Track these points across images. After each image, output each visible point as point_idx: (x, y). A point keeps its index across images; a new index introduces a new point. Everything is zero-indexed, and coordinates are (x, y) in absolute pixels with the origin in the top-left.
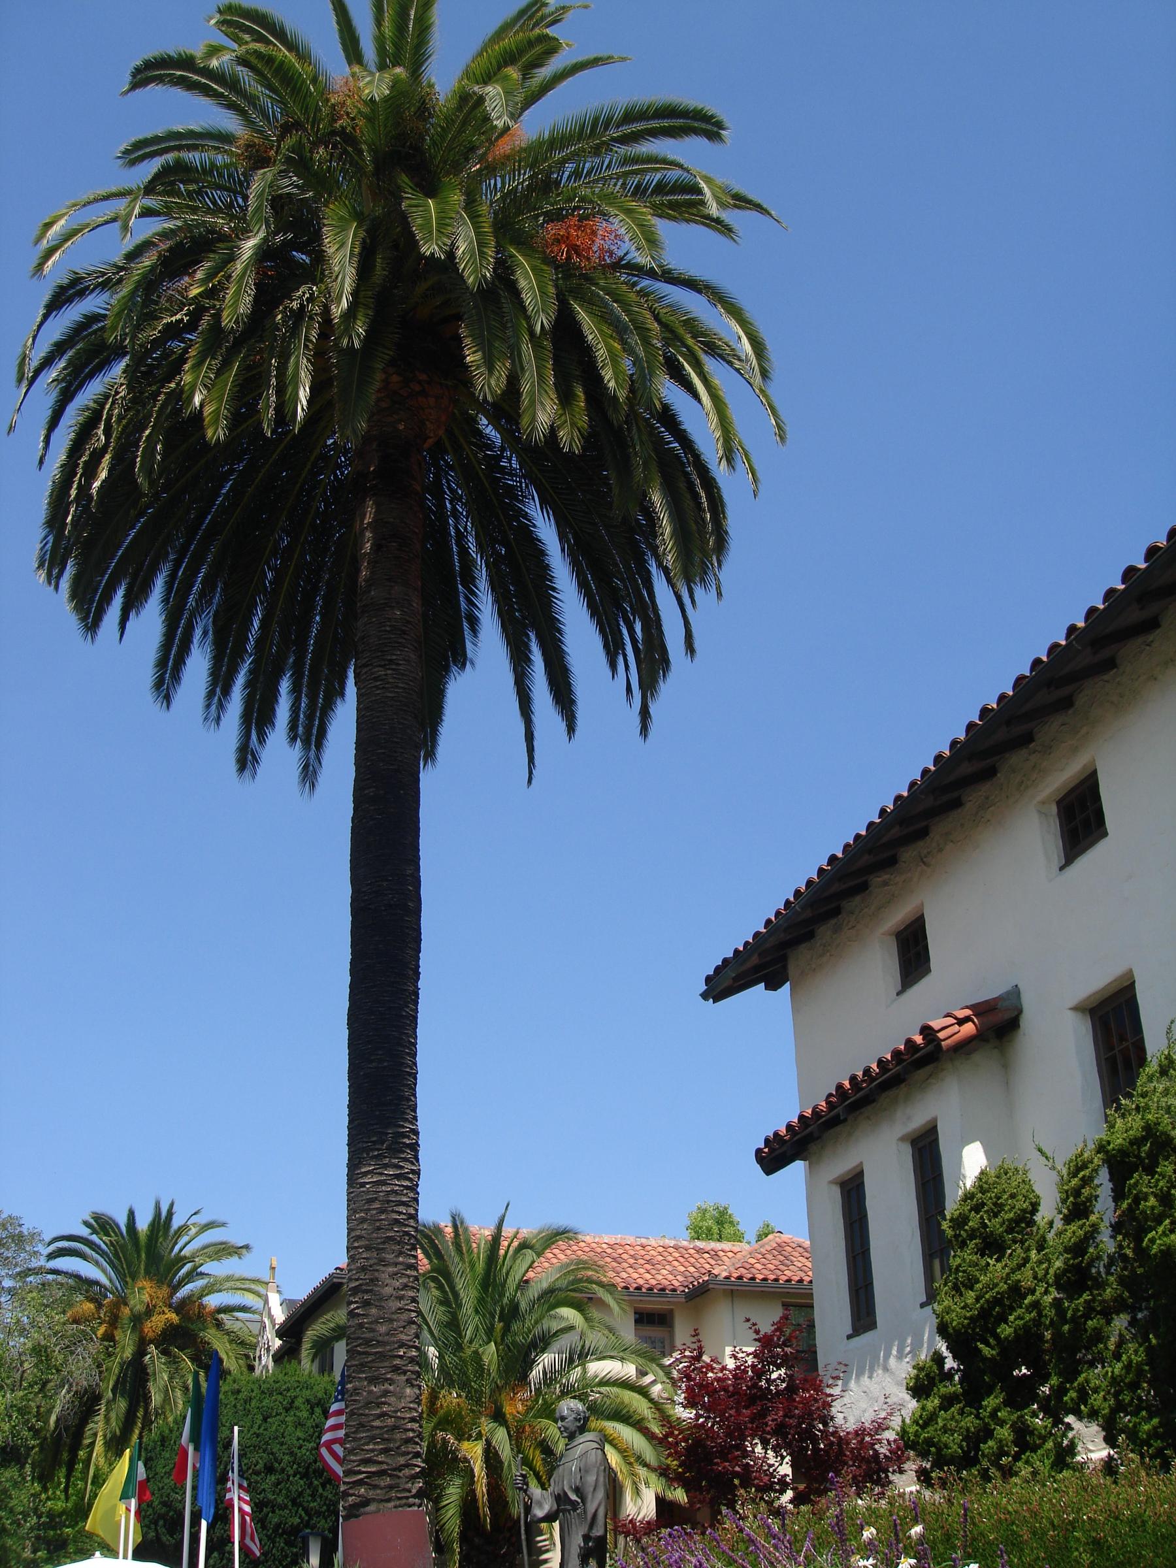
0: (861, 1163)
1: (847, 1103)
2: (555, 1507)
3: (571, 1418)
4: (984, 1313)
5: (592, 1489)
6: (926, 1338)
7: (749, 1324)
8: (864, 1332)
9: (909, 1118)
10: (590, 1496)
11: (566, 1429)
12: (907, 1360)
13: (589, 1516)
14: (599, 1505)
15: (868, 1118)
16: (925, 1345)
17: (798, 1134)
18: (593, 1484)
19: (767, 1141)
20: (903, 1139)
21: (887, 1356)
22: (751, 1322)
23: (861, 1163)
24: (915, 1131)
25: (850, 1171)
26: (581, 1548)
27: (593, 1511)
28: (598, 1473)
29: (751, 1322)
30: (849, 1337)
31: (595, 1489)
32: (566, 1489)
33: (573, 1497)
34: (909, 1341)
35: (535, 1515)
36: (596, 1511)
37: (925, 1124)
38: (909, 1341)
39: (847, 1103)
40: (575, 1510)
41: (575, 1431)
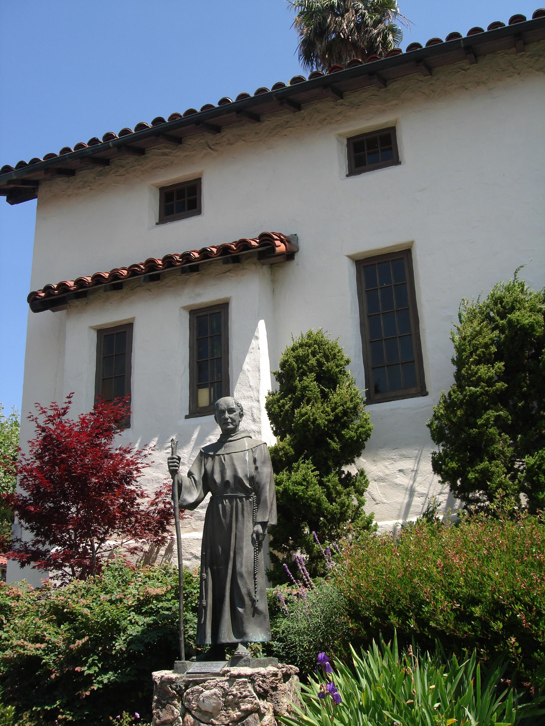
0: (134, 319)
4: (337, 418)
6: (195, 436)
9: (199, 295)
16: (192, 443)
20: (184, 308)
23: (134, 319)
25: (114, 323)
32: (241, 474)
40: (248, 498)
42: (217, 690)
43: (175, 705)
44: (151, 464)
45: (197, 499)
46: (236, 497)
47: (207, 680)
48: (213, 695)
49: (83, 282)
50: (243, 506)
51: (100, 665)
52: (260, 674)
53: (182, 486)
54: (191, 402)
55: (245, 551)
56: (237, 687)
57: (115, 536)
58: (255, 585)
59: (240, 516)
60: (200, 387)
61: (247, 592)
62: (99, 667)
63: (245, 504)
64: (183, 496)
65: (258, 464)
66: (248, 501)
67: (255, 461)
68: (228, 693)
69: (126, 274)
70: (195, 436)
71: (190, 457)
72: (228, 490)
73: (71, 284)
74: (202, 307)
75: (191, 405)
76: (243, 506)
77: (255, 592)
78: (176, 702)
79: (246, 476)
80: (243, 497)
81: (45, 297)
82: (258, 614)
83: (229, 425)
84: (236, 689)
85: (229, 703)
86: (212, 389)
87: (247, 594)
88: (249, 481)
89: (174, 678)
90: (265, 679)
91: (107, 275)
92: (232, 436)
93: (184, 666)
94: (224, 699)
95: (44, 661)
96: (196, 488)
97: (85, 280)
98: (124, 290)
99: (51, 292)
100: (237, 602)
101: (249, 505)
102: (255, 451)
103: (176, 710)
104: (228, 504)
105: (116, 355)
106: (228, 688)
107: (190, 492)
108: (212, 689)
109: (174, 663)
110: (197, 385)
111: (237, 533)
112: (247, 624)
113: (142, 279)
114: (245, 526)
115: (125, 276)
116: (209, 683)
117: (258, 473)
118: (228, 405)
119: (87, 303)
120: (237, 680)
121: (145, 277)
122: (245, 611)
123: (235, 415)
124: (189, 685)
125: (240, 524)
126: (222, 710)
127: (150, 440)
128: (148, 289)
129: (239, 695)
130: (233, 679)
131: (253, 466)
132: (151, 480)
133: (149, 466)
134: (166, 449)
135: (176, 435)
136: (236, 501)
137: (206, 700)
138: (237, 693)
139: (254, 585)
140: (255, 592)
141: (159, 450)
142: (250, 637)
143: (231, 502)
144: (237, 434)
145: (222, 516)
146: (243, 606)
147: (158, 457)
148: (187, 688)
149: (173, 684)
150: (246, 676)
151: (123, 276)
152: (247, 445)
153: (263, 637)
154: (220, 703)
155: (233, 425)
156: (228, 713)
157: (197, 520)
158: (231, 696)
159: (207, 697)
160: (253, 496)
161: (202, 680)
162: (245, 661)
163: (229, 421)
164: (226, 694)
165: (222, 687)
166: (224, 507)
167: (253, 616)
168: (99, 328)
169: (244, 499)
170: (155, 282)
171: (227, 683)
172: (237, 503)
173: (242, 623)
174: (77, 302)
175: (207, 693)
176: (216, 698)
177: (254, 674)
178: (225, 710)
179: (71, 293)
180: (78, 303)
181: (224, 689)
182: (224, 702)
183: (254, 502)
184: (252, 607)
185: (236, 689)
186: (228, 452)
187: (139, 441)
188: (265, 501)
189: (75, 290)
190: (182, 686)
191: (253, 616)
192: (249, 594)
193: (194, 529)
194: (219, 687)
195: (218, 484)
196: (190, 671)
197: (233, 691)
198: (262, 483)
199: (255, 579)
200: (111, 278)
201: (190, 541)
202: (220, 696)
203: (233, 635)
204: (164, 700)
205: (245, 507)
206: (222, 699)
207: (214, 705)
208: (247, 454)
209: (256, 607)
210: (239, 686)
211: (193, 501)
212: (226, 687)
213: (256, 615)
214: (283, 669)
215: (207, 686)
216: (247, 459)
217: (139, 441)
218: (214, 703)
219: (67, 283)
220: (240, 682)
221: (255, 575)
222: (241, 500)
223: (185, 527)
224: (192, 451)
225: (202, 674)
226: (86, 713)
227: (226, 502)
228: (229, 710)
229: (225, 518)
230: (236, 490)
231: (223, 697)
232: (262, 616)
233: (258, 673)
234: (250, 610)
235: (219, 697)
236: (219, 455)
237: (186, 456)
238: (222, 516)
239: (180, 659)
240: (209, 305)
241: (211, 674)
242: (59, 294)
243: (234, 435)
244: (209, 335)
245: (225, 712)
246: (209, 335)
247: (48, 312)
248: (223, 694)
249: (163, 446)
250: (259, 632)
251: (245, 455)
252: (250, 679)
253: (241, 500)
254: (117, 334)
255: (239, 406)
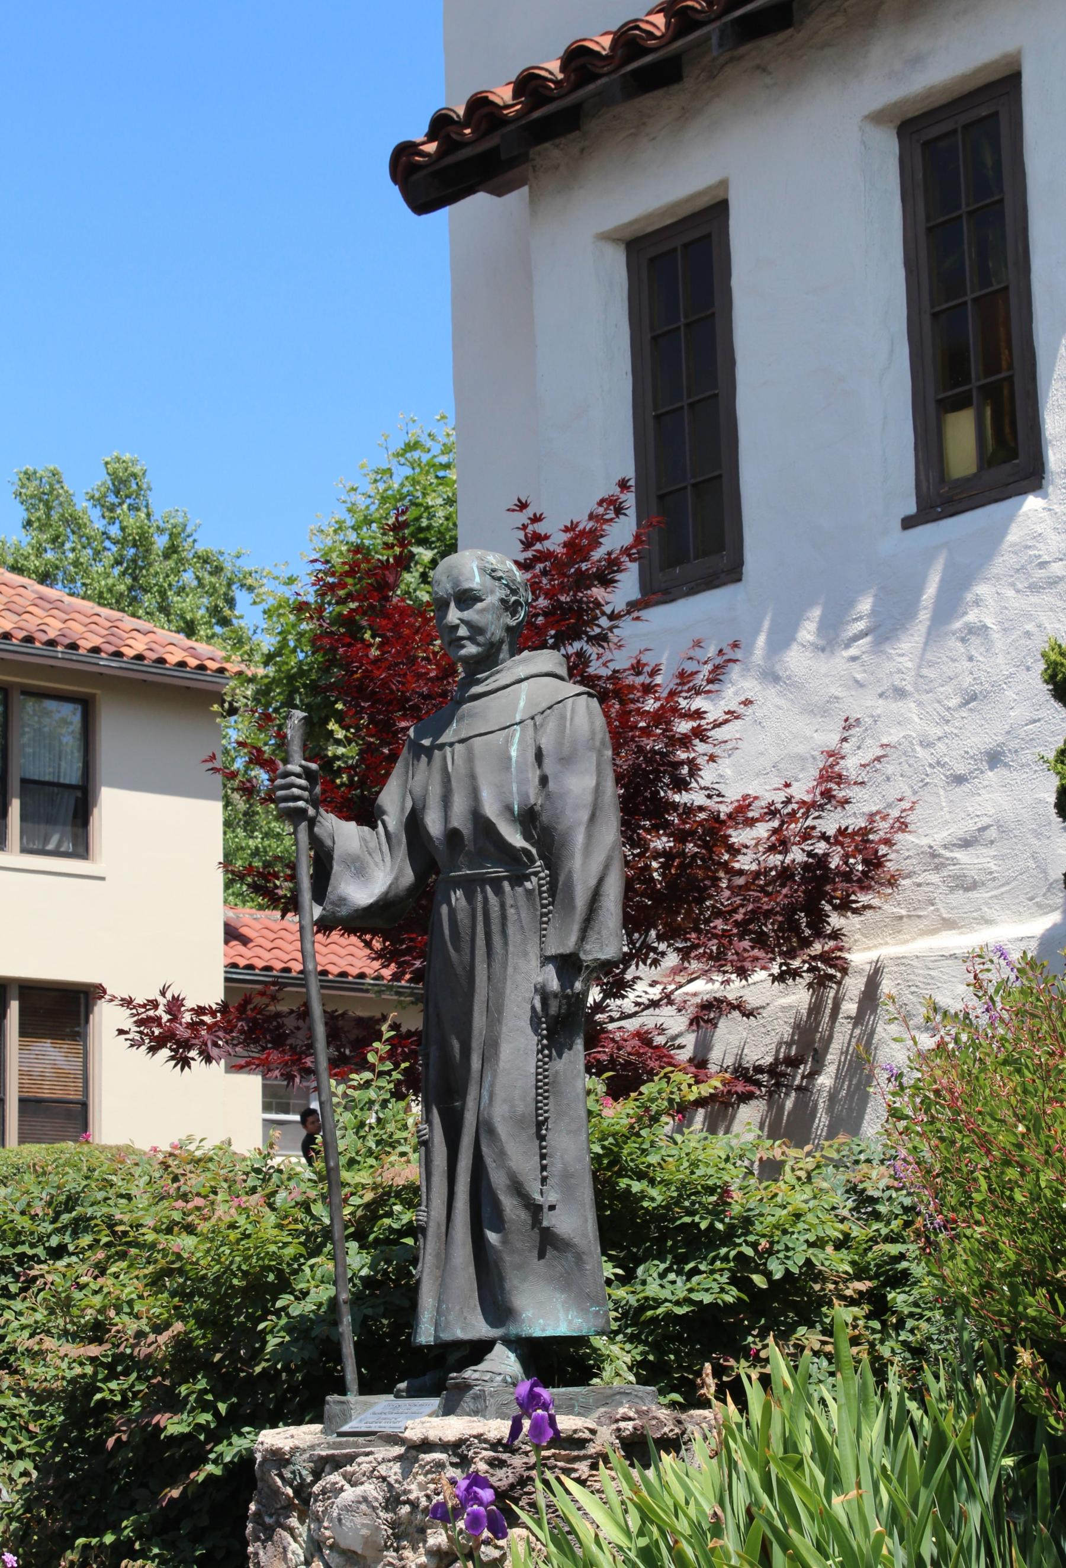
0: (724, 184)
1: (630, 67)
2: (409, 877)
3: (492, 600)
5: (584, 816)
6: (931, 591)
7: (522, 518)
8: (693, 591)
9: (917, 61)
10: (579, 838)
11: (476, 630)
12: (853, 651)
13: (581, 900)
14: (606, 867)
15: (763, 69)
16: (924, 616)
17: (550, 100)
18: (589, 798)
19: (441, 124)
20: (878, 118)
21: (781, 640)
22: (529, 512)
23: (724, 184)
24: (929, 93)
26: (545, 995)
27: (593, 882)
28: (598, 764)
29: (529, 512)
30: (908, 523)
31: (593, 818)
32: (491, 809)
33: (516, 839)
34: (865, 605)
35: (342, 901)
36: (601, 881)
37: (965, 78)
38: (865, 605)
39: (630, 67)
40: (517, 880)
41: (501, 642)
42: (372, 1486)
43: (291, 1530)
44: (741, 710)
45: (386, 893)
46: (482, 880)
47: (357, 1455)
48: (360, 1502)
49: (540, 82)
50: (503, 906)
51: (222, 1407)
52: (486, 1441)
53: (330, 858)
54: (921, 467)
55: (506, 1051)
56: (421, 1478)
57: (672, 959)
58: (543, 1157)
59: (497, 940)
60: (959, 404)
61: (508, 1182)
62: (216, 1414)
63: (509, 902)
64: (335, 888)
65: (550, 766)
66: (520, 890)
67: (539, 756)
68: (398, 1495)
69: (663, 28)
70: (931, 591)
71: (920, 667)
72: (461, 859)
73: (504, 94)
74: (937, 104)
75: (923, 477)
76: (503, 906)
77: (544, 1180)
78: (293, 1522)
79: (509, 808)
80: (500, 880)
81: (441, 153)
82: (556, 1248)
83: (463, 647)
84: (419, 1484)
85: (402, 1528)
86: (988, 412)
87: (508, 1187)
88: (522, 824)
89: (287, 1448)
90: (504, 1456)
91: (607, 41)
92: (479, 682)
93: (343, 1412)
94: (389, 1516)
95: (98, 1396)
96: (388, 858)
97: (543, 73)
98: (688, 83)
99: (454, 136)
100: (486, 1212)
101: (522, 901)
102: (542, 725)
103: (294, 1546)
104: (463, 902)
105: (687, 325)
106: (397, 1481)
107: (360, 870)
108: (362, 1483)
109: (323, 1402)
110: (939, 402)
111: (491, 994)
112: (516, 1282)
113: (714, 40)
114: (510, 970)
115: (663, 36)
116: (359, 1464)
117: (548, 796)
118: (456, 583)
119: (582, 151)
120: (422, 1456)
121: (722, 31)
122: (505, 1242)
123: (481, 611)
124: (323, 1471)
125: (496, 966)
126: (387, 1548)
127: (851, 603)
128: (758, 67)
129: (424, 1502)
130: (414, 1453)
131: (533, 776)
132: (811, 760)
133: (737, 718)
134: (847, 646)
135: (873, 591)
136: (484, 892)
137: (345, 1516)
138: (418, 1498)
139: (537, 1158)
140: (544, 1180)
141: (828, 649)
142: (527, 1323)
143: (470, 897)
144: (498, 672)
145: (449, 944)
146: (499, 1225)
147: (826, 675)
148: (317, 1475)
149: (285, 1467)
150: (443, 1446)
151: (655, 38)
152: (522, 704)
153: (570, 1322)
154: (378, 1528)
155: (478, 644)
156: (401, 1559)
157: (952, 889)
158: (407, 1506)
159: (347, 1508)
160: (536, 874)
161: (346, 1455)
162: (476, 1398)
163: (463, 631)
164: (393, 1501)
165: (384, 1479)
166: (452, 912)
167: (541, 1255)
168: (628, 235)
169: (506, 885)
170: (781, 37)
171: (397, 1467)
172: (486, 900)
173: (501, 1279)
174: (551, 152)
175: (350, 1494)
176: (369, 1511)
177: (467, 1440)
178: (396, 1550)
179: (512, 127)
180: (556, 153)
181: (389, 1485)
182: (393, 1525)
183: (541, 893)
184: (533, 1227)
185: (419, 1484)
186: (463, 736)
187: (766, 625)
188: (569, 886)
189: (520, 115)
190: (304, 1473)
191: (541, 1255)
192: (518, 1189)
193: (944, 919)
194: (377, 1478)
195: (437, 843)
196: (346, 1428)
197: (410, 1492)
198: (562, 827)
199: (542, 1138)
200: (619, 52)
201: (931, 965)
202: (376, 1504)
203: (481, 1318)
204: (271, 1516)
205: (511, 912)
206: (382, 1514)
207: (364, 1532)
208: (518, 735)
209: (548, 1228)
210: (426, 1475)
211: (371, 901)
212: (392, 1480)
213: (550, 1253)
214: (622, 1425)
215: (354, 1473)
216: (514, 753)
217: (766, 625)
218: (363, 1525)
219: (492, 97)
220: (428, 1463)
221: (539, 1125)
222: (499, 891)
223: (919, 917)
224: (926, 644)
225: (361, 1440)
226: (198, 1553)
227: (458, 897)
228: (404, 1548)
229: (457, 949)
230: (479, 857)
231: (386, 1509)
232: (569, 1255)
233: (478, 1437)
234: (524, 1241)
235: (374, 1508)
236: (441, 747)
237: (910, 665)
238: (449, 944)
239: (343, 1392)
240: (955, 95)
241: (380, 1437)
242: (478, 139)
243: (486, 678)
244: (964, 209)
245: (394, 1554)
246: (964, 209)
247: (479, 202)
248: (387, 1500)
249: (838, 636)
250: (559, 1306)
251: (508, 741)
252: (455, 1454)
253: (499, 891)
254: (685, 246)
255: (500, 579)
